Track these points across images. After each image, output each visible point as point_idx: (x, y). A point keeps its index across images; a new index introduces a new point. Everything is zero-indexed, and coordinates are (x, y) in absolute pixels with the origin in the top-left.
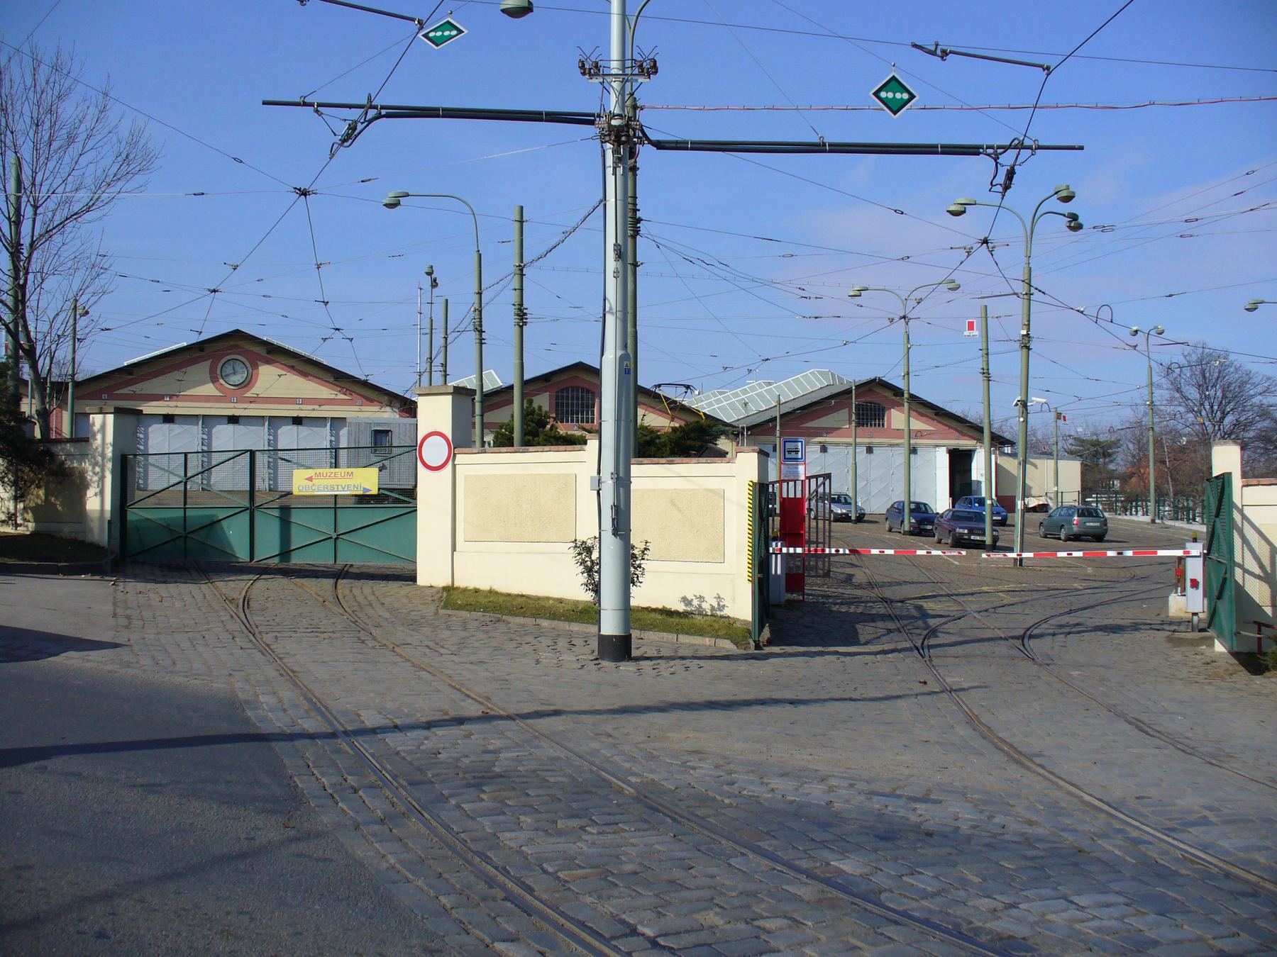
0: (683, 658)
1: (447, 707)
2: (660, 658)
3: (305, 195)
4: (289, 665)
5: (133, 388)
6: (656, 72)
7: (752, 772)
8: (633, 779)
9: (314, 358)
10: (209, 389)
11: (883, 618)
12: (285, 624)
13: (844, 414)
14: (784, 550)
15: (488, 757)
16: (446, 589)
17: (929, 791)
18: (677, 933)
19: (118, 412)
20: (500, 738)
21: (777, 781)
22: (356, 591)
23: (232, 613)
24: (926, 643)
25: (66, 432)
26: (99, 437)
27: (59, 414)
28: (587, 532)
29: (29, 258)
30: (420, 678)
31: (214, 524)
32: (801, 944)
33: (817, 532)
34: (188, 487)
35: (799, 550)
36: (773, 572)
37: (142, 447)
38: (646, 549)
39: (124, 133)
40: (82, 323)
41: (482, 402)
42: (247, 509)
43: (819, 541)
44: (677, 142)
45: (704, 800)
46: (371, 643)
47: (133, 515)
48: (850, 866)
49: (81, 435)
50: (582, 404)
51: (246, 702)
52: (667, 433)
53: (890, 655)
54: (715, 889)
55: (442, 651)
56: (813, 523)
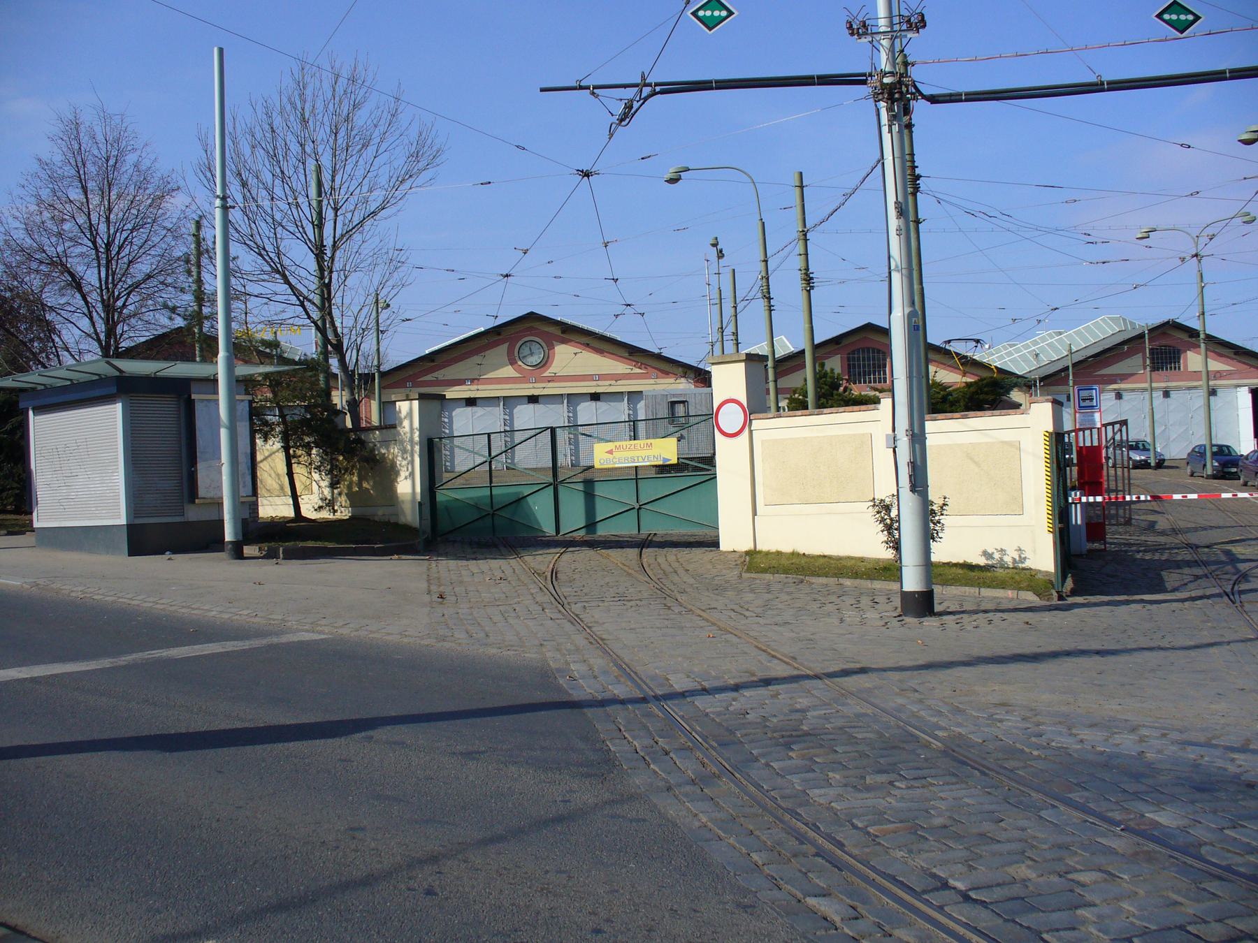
0: (986, 611)
1: (753, 668)
2: (963, 612)
3: (588, 176)
4: (598, 633)
5: (435, 374)
6: (924, 26)
7: (1060, 723)
8: (940, 734)
9: (608, 334)
10: (508, 371)
11: (1189, 564)
12: (593, 594)
13: (1137, 359)
14: (1084, 499)
15: (797, 716)
16: (748, 553)
17: (1248, 741)
18: (989, 887)
19: (422, 397)
20: (807, 697)
21: (1086, 732)
22: (661, 560)
23: (541, 585)
24: (1236, 588)
25: (375, 420)
26: (406, 423)
27: (368, 404)
28: (885, 489)
29: (332, 258)
30: (727, 641)
31: (520, 500)
32: (1118, 899)
33: (1116, 480)
34: (493, 467)
35: (1099, 499)
36: (1074, 522)
37: (447, 431)
38: (944, 505)
39: (413, 134)
40: (384, 315)
41: (775, 368)
42: (551, 484)
43: (1119, 489)
44: (951, 95)
45: (1012, 752)
46: (677, 609)
47: (441, 496)
48: (1166, 818)
49: (388, 423)
50: (874, 364)
51: (558, 670)
52: (960, 388)
53: (1197, 602)
54: (1026, 842)
55: (747, 614)
56: (1112, 472)
